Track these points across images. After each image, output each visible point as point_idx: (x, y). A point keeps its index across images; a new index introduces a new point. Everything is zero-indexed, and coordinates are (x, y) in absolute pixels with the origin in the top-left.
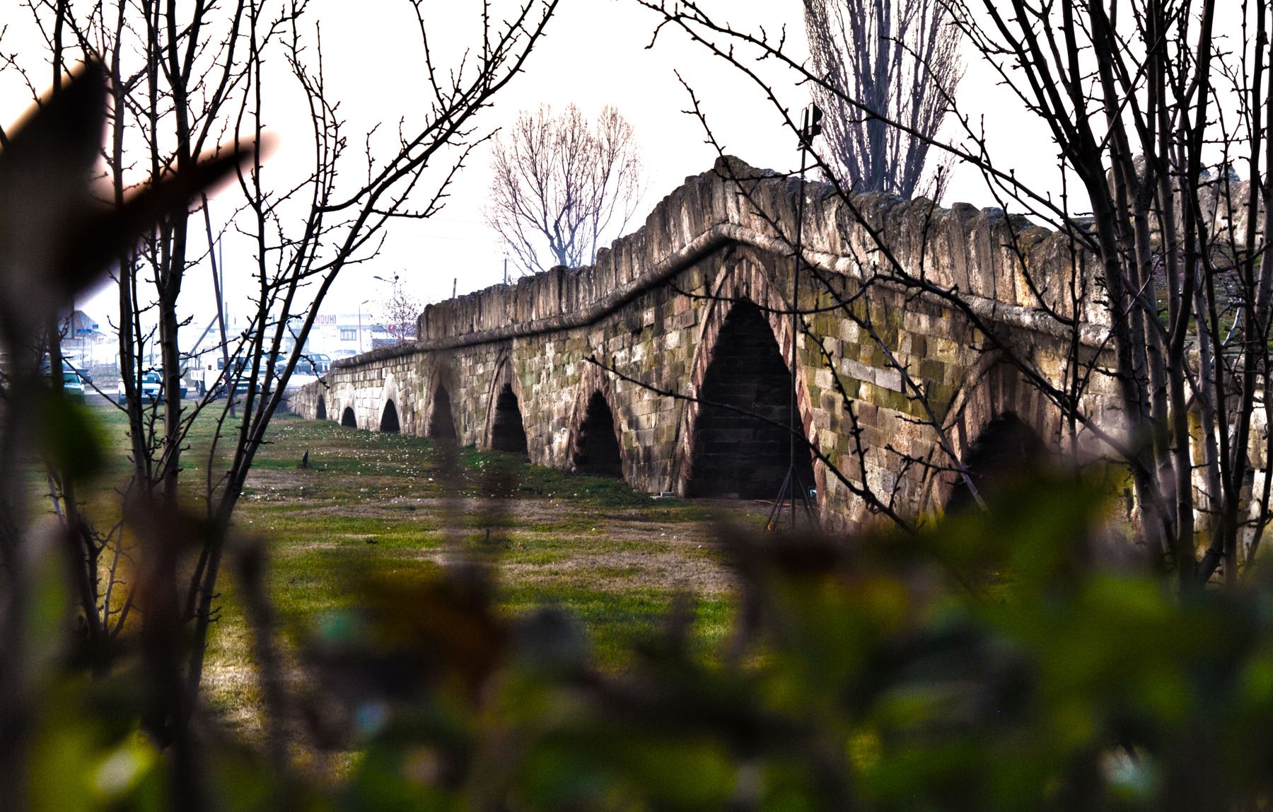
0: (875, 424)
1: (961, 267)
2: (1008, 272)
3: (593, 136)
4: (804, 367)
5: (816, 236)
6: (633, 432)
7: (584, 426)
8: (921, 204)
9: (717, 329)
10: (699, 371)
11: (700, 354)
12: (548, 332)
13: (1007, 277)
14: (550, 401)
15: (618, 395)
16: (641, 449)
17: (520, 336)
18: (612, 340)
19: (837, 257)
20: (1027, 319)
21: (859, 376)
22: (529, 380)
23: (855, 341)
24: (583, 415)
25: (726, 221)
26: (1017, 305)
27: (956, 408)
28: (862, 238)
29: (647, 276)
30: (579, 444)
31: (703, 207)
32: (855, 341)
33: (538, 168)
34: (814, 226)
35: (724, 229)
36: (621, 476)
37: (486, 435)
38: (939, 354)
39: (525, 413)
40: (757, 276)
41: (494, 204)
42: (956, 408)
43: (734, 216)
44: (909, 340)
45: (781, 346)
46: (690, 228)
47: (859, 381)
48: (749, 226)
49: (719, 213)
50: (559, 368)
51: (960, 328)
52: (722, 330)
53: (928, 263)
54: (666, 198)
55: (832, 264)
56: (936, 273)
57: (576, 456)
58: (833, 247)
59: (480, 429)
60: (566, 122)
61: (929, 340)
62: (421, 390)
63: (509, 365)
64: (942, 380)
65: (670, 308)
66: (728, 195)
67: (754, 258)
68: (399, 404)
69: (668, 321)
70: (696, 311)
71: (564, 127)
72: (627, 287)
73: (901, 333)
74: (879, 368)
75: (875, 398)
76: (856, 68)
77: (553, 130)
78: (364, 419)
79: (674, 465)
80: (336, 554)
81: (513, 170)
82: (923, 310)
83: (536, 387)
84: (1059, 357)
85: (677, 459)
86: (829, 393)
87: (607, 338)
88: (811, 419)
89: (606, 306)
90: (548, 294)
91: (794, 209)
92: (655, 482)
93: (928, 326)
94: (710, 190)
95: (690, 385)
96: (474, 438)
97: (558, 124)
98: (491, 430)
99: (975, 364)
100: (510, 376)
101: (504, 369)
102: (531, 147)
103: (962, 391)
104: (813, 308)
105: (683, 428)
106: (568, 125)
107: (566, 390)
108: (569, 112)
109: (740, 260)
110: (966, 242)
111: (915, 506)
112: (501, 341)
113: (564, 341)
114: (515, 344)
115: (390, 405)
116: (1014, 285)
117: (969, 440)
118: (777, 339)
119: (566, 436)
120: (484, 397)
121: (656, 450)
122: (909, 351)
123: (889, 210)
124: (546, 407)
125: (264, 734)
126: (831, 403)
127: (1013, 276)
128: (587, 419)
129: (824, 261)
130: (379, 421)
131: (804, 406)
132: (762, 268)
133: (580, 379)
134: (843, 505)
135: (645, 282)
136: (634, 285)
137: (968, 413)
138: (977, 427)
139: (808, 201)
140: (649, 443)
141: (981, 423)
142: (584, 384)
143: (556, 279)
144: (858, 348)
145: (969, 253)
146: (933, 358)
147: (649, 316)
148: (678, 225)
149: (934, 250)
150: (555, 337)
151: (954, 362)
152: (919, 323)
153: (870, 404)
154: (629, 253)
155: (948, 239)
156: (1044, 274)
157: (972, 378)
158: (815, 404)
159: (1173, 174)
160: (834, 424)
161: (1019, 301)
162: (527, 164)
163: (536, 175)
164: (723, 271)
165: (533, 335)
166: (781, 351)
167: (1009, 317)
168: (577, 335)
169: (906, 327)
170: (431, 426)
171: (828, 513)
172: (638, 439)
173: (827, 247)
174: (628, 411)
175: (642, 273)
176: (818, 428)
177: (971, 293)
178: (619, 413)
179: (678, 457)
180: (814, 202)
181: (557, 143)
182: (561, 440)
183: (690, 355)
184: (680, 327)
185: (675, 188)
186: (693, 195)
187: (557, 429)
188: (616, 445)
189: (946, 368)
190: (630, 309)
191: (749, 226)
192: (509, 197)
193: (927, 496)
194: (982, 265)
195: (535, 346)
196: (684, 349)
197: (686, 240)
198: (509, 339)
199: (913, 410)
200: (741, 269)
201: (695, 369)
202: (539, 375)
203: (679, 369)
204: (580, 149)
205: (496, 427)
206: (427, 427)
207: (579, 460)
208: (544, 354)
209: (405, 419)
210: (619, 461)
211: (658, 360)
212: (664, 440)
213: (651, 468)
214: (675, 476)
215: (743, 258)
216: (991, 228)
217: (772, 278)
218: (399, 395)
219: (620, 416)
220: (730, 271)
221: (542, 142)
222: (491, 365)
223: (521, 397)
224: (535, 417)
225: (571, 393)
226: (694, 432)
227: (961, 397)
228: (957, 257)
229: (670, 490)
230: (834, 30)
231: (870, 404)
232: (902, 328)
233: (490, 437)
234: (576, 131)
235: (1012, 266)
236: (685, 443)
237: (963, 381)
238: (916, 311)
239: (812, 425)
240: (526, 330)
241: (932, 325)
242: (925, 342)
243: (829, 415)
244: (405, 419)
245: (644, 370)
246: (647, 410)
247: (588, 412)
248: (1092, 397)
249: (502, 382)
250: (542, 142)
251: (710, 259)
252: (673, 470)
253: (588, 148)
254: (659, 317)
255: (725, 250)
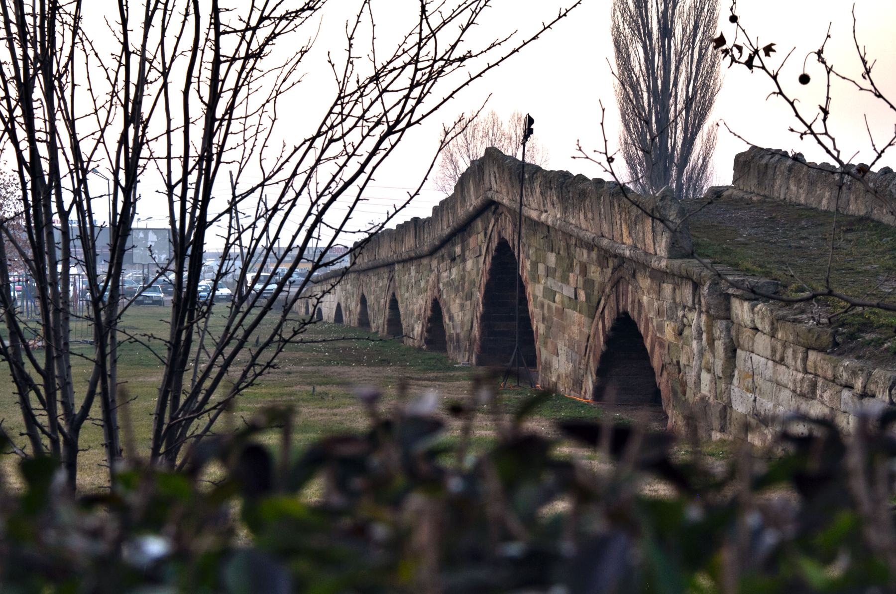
0: (562, 319)
1: (597, 219)
2: (619, 222)
3: (506, 131)
4: (530, 283)
5: (531, 199)
6: (451, 323)
8: (579, 179)
9: (490, 258)
11: (482, 274)
12: (411, 259)
13: (618, 226)
14: (413, 304)
15: (444, 300)
16: (455, 335)
17: (398, 262)
18: (441, 265)
19: (542, 212)
20: (627, 253)
21: (555, 289)
22: (403, 289)
23: (554, 266)
24: (429, 313)
25: (490, 189)
26: (624, 244)
27: (600, 310)
32: (554, 266)
33: (471, 152)
35: (489, 194)
36: (446, 351)
37: (384, 325)
38: (592, 274)
39: (402, 311)
41: (442, 176)
42: (600, 310)
43: (495, 187)
44: (578, 265)
48: (501, 193)
49: (487, 185)
50: (418, 282)
51: (601, 258)
52: (493, 259)
53: (582, 217)
55: (539, 217)
57: (426, 339)
59: (381, 321)
60: (489, 123)
61: (588, 266)
62: (353, 297)
63: (394, 281)
65: (468, 244)
67: (506, 213)
68: (343, 305)
69: (467, 253)
70: (480, 246)
71: (487, 126)
72: (447, 231)
75: (562, 302)
76: (648, 87)
77: (480, 128)
78: (326, 314)
79: (470, 345)
80: (262, 408)
81: (454, 154)
82: (584, 246)
83: (407, 295)
85: (471, 341)
87: (439, 264)
89: (437, 243)
90: (410, 235)
92: (461, 356)
94: (483, 169)
95: (478, 294)
96: (378, 327)
97: (483, 124)
98: (386, 323)
100: (395, 288)
101: (392, 283)
102: (466, 139)
103: (603, 298)
105: (475, 318)
106: (490, 125)
107: (420, 296)
108: (490, 116)
109: (501, 214)
110: (599, 204)
112: (390, 265)
113: (419, 265)
114: (397, 267)
115: (339, 305)
116: (622, 231)
117: (607, 330)
119: (421, 326)
120: (382, 301)
121: (462, 336)
122: (578, 273)
123: (564, 183)
124: (411, 307)
125: (674, 444)
127: (621, 225)
128: (432, 316)
129: (534, 215)
130: (333, 316)
131: (531, 307)
133: (426, 290)
134: (548, 371)
137: (606, 312)
139: (527, 176)
140: (459, 331)
142: (429, 293)
143: (413, 226)
144: (555, 270)
145: (600, 210)
146: (589, 277)
147: (458, 250)
148: (469, 192)
149: (584, 208)
150: (415, 262)
153: (560, 306)
155: (591, 202)
156: (636, 224)
157: (607, 290)
158: (535, 307)
159: (200, 201)
161: (624, 241)
162: (463, 150)
163: (469, 157)
164: (493, 221)
165: (406, 261)
168: (425, 261)
170: (359, 319)
174: (449, 311)
175: (453, 222)
177: (603, 236)
178: (444, 310)
179: (473, 340)
180: (529, 177)
181: (482, 137)
182: (418, 329)
183: (478, 275)
184: (473, 256)
185: (774, 147)
186: (474, 172)
187: (416, 322)
188: (443, 332)
190: (449, 245)
191: (501, 193)
192: (452, 171)
193: (587, 365)
195: (406, 269)
196: (475, 271)
197: (473, 201)
198: (393, 264)
200: (501, 219)
202: (408, 287)
203: (473, 283)
204: (497, 140)
205: (389, 320)
206: (356, 321)
208: (410, 274)
209: (346, 315)
210: (445, 343)
211: (463, 278)
212: (465, 329)
213: (459, 347)
214: (471, 352)
216: (610, 194)
218: (343, 300)
219: (445, 314)
220: (496, 221)
221: (473, 136)
222: (386, 281)
223: (399, 301)
224: (405, 314)
225: (423, 299)
226: (480, 324)
227: (602, 302)
228: (595, 213)
229: (468, 361)
230: (635, 63)
231: (560, 306)
233: (386, 326)
234: (495, 129)
235: (620, 219)
236: (476, 332)
237: (603, 292)
240: (400, 259)
241: (589, 256)
242: (586, 267)
244: (346, 315)
245: (456, 284)
246: (457, 310)
247: (432, 311)
248: (661, 302)
249: (391, 292)
250: (473, 136)
251: (486, 213)
252: (470, 348)
253: (503, 139)
254: (463, 251)
255: (493, 207)
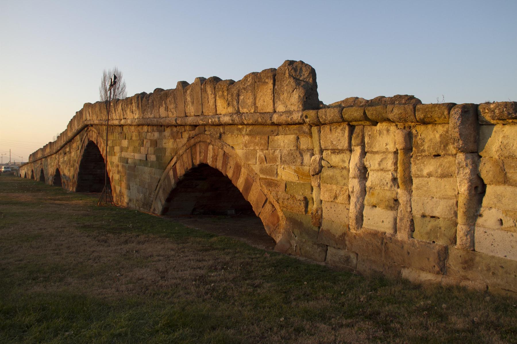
7: (55, 176)
10: (79, 161)
17: (44, 158)
28: (131, 110)
29: (67, 140)
30: (54, 180)
31: (80, 118)
34: (113, 112)
35: (86, 122)
40: (94, 134)
44: (149, 142)
45: (101, 152)
46: (77, 125)
47: (128, 158)
54: (71, 120)
55: (119, 122)
56: (166, 113)
57: (53, 182)
58: (120, 116)
64: (165, 154)
66: (87, 113)
73: (145, 141)
74: (136, 153)
84: (243, 135)
86: (117, 163)
88: (110, 171)
91: (107, 109)
93: (158, 136)
99: (183, 146)
104: (124, 128)
109: (90, 131)
111: (152, 199)
118: (100, 150)
122: (149, 146)
126: (118, 166)
132: (96, 131)
135: (67, 141)
136: (64, 142)
138: (183, 170)
141: (185, 168)
142: (55, 167)
146: (161, 147)
151: (172, 147)
152: (154, 135)
154: (63, 135)
158: (112, 166)
160: (119, 172)
166: (101, 153)
167: (213, 120)
169: (148, 138)
171: (116, 199)
172: (65, 178)
173: (118, 118)
175: (66, 139)
176: (113, 174)
189: (167, 149)
190: (63, 149)
194: (195, 102)
196: (75, 156)
199: (151, 166)
201: (78, 161)
207: (54, 183)
211: (70, 160)
215: (91, 130)
217: (99, 133)
225: (52, 169)
227: (175, 159)
232: (146, 138)
237: (176, 153)
238: (153, 131)
239: (111, 173)
243: (117, 169)
249: (41, 167)
254: (70, 150)
